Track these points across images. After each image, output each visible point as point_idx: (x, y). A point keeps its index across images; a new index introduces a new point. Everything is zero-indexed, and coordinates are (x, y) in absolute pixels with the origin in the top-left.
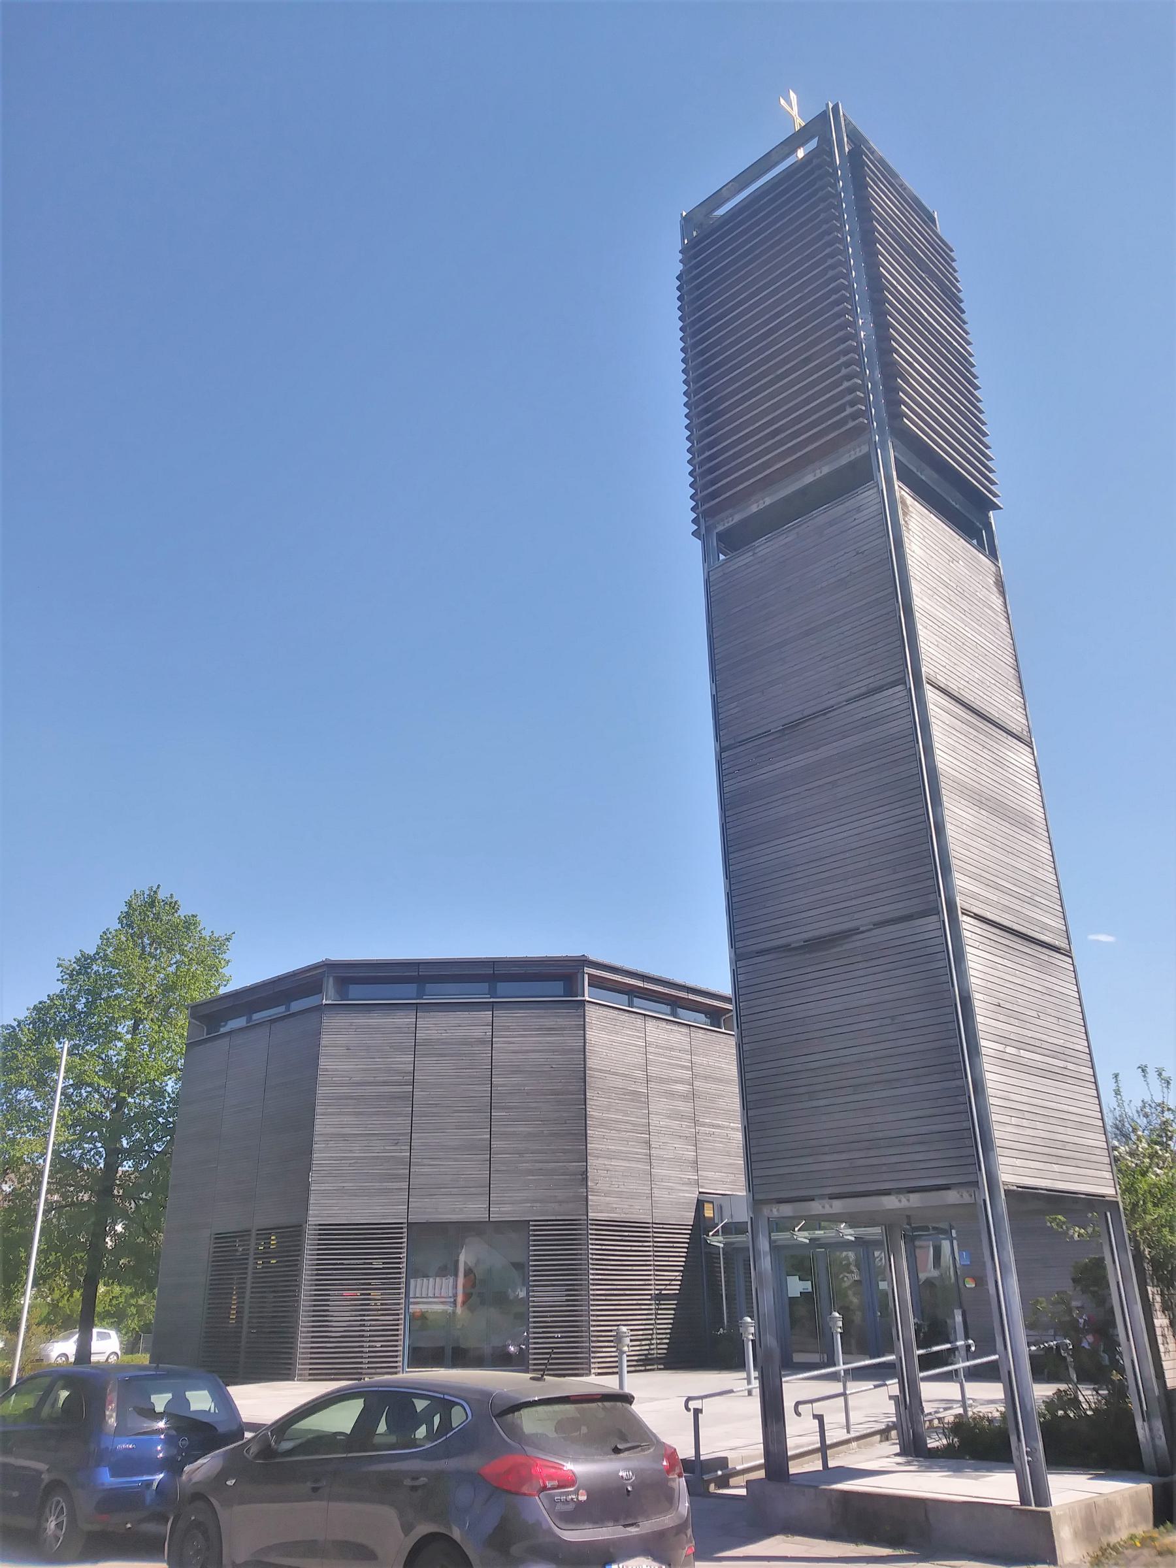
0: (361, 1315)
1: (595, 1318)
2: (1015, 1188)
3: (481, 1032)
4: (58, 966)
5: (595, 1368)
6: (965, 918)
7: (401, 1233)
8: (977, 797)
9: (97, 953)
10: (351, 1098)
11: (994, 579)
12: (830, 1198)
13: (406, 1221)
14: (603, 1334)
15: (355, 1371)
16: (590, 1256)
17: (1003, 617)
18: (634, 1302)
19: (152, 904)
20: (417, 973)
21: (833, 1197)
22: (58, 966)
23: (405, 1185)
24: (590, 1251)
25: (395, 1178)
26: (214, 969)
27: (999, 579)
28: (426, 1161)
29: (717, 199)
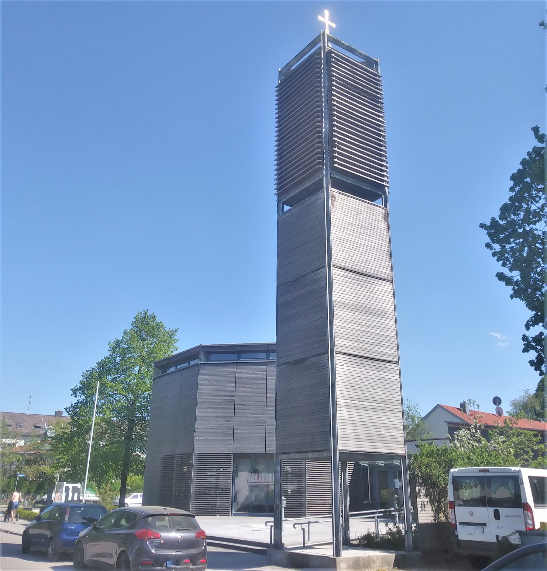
0: (215, 490)
1: (308, 494)
2: (346, 451)
3: (262, 374)
4: (108, 345)
5: (308, 515)
6: (338, 355)
7: (231, 457)
8: (354, 307)
9: (122, 340)
10: (210, 402)
11: (383, 216)
12: (295, 453)
13: (232, 452)
14: (312, 501)
15: (212, 512)
16: (306, 468)
17: (385, 231)
18: (328, 488)
19: (145, 318)
20: (236, 350)
21: (296, 453)
22: (108, 345)
23: (232, 438)
24: (307, 467)
25: (227, 435)
26: (169, 345)
27: (386, 215)
28: (240, 428)
29: (289, 65)
